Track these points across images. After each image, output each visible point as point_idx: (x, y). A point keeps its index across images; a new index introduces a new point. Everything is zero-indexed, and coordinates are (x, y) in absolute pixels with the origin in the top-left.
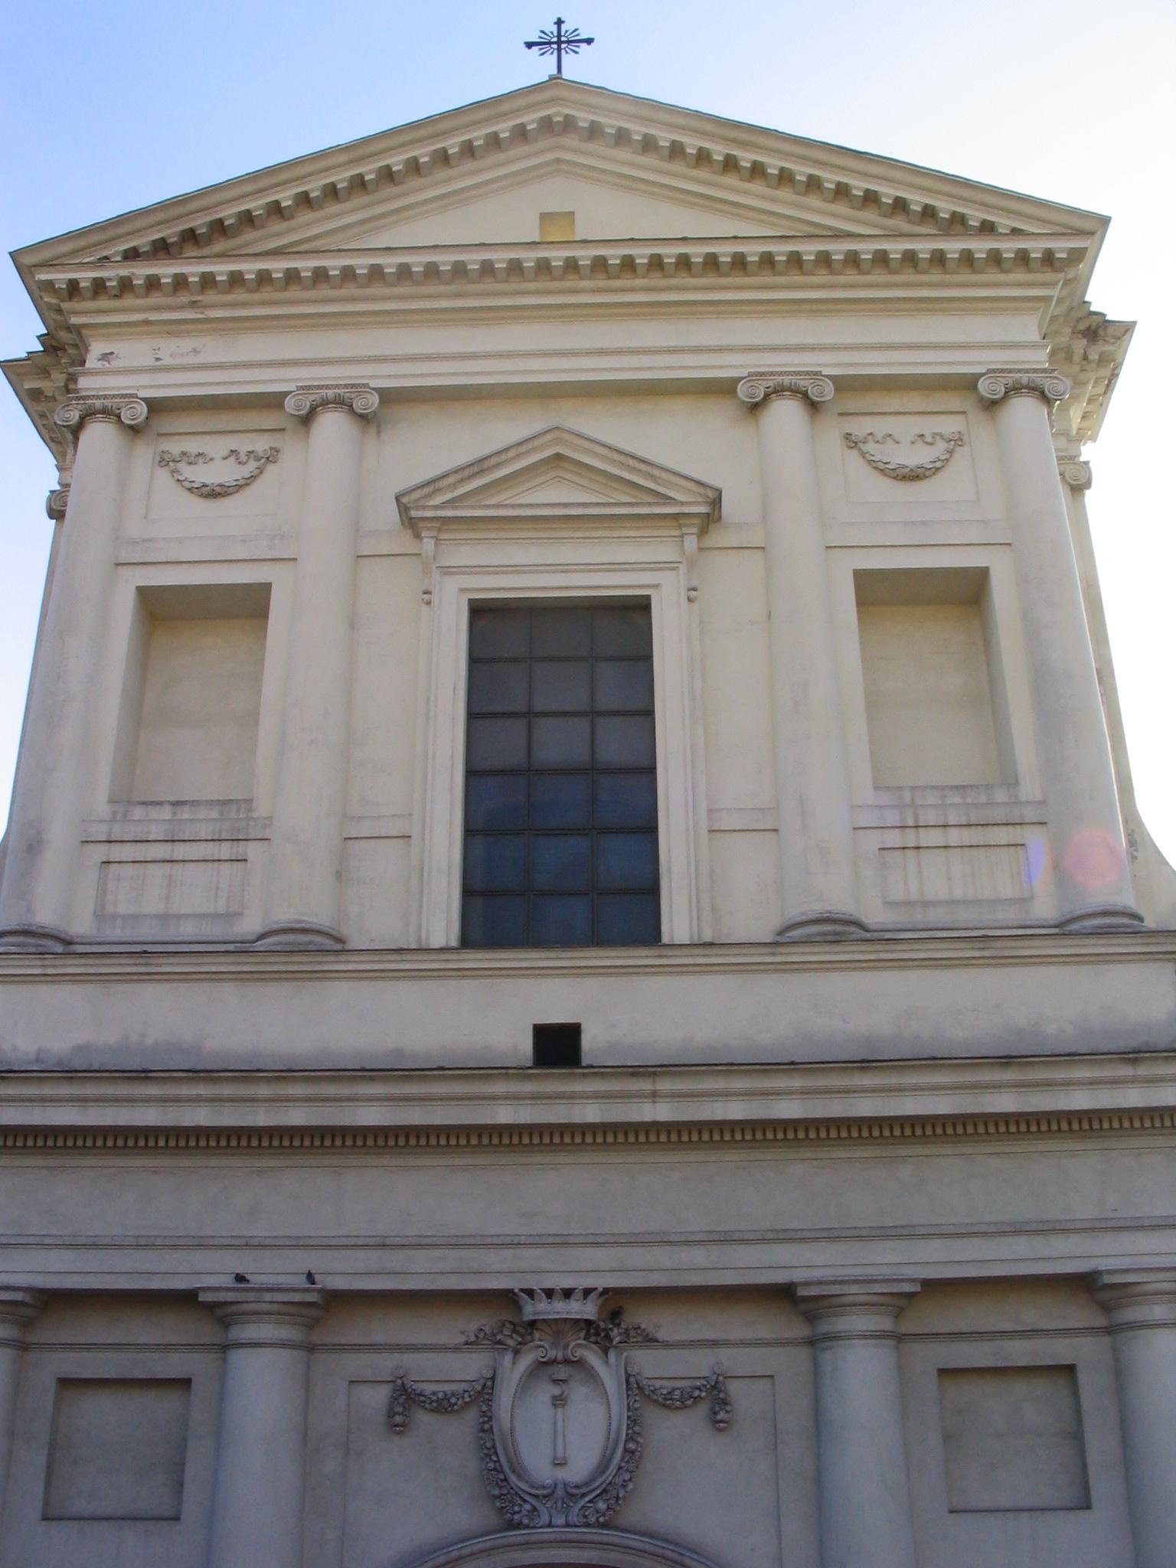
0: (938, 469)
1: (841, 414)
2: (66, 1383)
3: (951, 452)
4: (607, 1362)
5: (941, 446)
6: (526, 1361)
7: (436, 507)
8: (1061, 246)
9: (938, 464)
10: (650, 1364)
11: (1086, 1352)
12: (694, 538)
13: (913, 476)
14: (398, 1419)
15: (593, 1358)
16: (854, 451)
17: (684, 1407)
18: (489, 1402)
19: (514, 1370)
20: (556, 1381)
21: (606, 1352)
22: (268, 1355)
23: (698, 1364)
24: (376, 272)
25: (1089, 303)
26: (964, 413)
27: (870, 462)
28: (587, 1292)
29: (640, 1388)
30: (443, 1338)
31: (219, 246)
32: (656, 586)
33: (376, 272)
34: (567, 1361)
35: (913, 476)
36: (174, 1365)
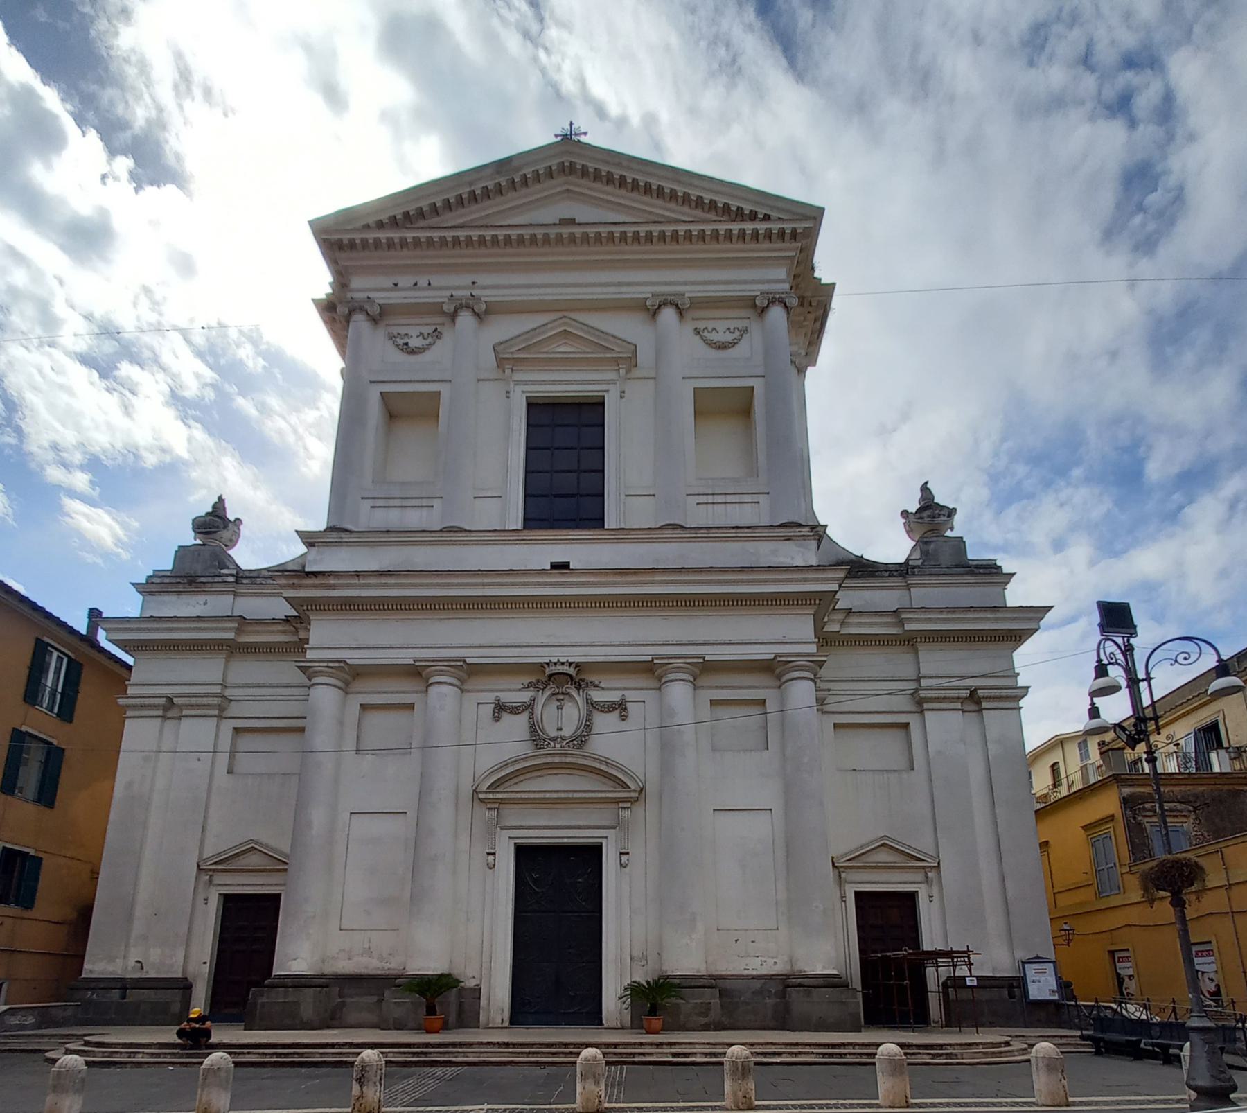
0: (735, 343)
1: (693, 319)
2: (364, 707)
3: (742, 336)
4: (579, 694)
5: (737, 333)
6: (548, 693)
7: (512, 353)
8: (800, 226)
9: (735, 341)
10: (597, 695)
11: (770, 695)
12: (624, 370)
13: (722, 346)
14: (496, 714)
15: (574, 693)
16: (698, 336)
17: (610, 711)
18: (532, 709)
19: (542, 698)
20: (558, 700)
21: (579, 690)
22: (444, 688)
23: (614, 696)
24: (508, 240)
25: (820, 279)
26: (749, 318)
27: (704, 341)
28: (571, 664)
29: (592, 705)
30: (513, 687)
31: (434, 221)
32: (607, 391)
33: (508, 240)
34: (563, 694)
35: (722, 346)
36: (407, 699)
